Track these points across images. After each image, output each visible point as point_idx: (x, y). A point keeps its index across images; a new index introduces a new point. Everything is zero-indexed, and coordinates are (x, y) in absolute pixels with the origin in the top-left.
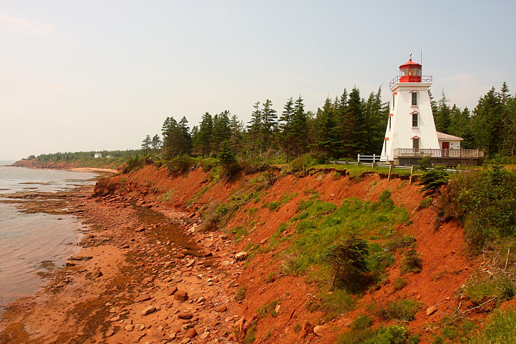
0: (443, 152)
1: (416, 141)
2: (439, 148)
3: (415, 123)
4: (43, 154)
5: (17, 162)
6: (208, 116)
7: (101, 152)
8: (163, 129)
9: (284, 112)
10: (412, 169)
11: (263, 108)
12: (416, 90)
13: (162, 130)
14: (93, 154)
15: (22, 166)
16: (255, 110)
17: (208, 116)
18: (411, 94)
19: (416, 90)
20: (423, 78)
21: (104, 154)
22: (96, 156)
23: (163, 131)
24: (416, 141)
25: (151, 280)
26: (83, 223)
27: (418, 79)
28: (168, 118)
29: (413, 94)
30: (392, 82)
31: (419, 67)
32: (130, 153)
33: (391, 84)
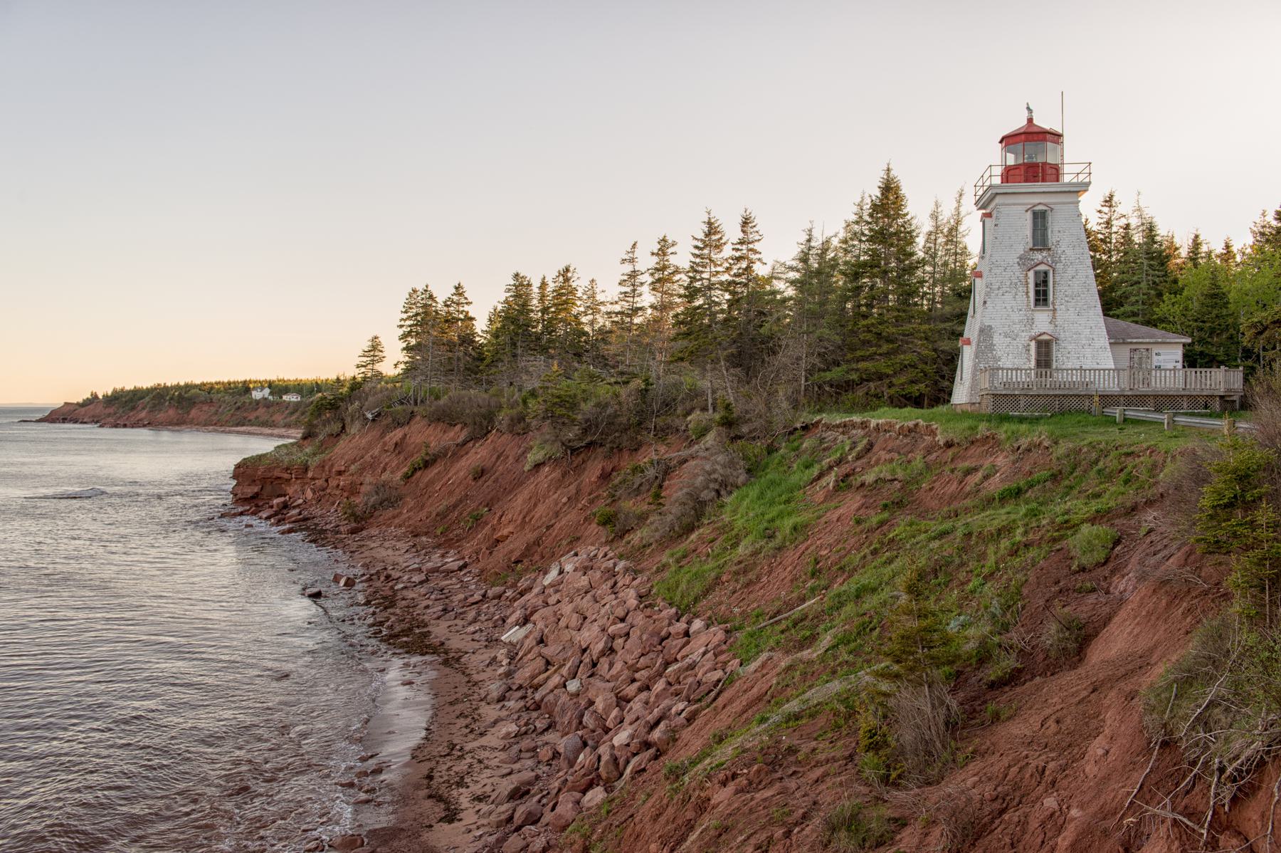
0: (1132, 377)
1: (1044, 350)
2: (1113, 367)
3: (1042, 297)
4: (119, 387)
5: (54, 412)
6: (520, 287)
7: (270, 385)
8: (402, 323)
9: (402, 320)
10: (1166, 421)
11: (653, 262)
12: (1045, 205)
13: (401, 326)
14: (245, 388)
15: (64, 420)
16: (628, 268)
17: (520, 287)
18: (1029, 215)
19: (1045, 205)
20: (1067, 169)
21: (278, 388)
22: (257, 395)
23: (404, 329)
24: (1044, 350)
25: (426, 669)
26: (883, 675)
27: (1052, 172)
28: (415, 291)
29: (1035, 214)
30: (980, 183)
31: (1056, 137)
32: (317, 387)
33: (1087, 170)
